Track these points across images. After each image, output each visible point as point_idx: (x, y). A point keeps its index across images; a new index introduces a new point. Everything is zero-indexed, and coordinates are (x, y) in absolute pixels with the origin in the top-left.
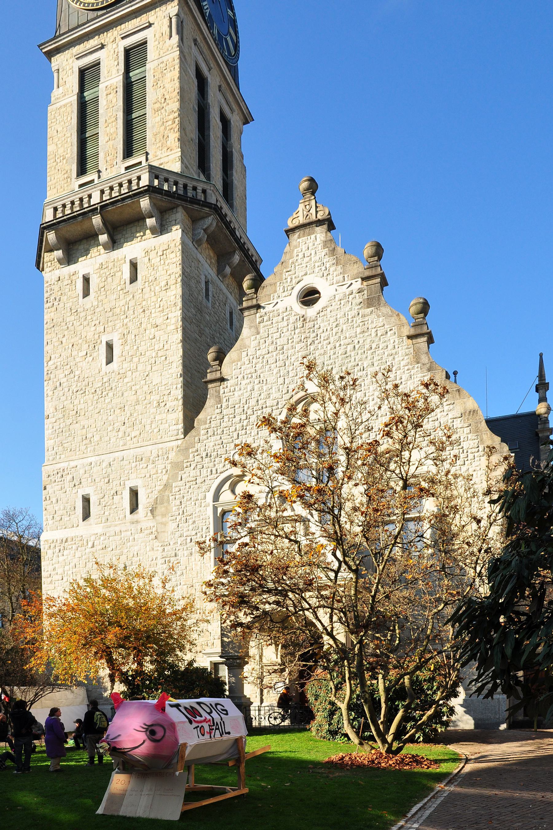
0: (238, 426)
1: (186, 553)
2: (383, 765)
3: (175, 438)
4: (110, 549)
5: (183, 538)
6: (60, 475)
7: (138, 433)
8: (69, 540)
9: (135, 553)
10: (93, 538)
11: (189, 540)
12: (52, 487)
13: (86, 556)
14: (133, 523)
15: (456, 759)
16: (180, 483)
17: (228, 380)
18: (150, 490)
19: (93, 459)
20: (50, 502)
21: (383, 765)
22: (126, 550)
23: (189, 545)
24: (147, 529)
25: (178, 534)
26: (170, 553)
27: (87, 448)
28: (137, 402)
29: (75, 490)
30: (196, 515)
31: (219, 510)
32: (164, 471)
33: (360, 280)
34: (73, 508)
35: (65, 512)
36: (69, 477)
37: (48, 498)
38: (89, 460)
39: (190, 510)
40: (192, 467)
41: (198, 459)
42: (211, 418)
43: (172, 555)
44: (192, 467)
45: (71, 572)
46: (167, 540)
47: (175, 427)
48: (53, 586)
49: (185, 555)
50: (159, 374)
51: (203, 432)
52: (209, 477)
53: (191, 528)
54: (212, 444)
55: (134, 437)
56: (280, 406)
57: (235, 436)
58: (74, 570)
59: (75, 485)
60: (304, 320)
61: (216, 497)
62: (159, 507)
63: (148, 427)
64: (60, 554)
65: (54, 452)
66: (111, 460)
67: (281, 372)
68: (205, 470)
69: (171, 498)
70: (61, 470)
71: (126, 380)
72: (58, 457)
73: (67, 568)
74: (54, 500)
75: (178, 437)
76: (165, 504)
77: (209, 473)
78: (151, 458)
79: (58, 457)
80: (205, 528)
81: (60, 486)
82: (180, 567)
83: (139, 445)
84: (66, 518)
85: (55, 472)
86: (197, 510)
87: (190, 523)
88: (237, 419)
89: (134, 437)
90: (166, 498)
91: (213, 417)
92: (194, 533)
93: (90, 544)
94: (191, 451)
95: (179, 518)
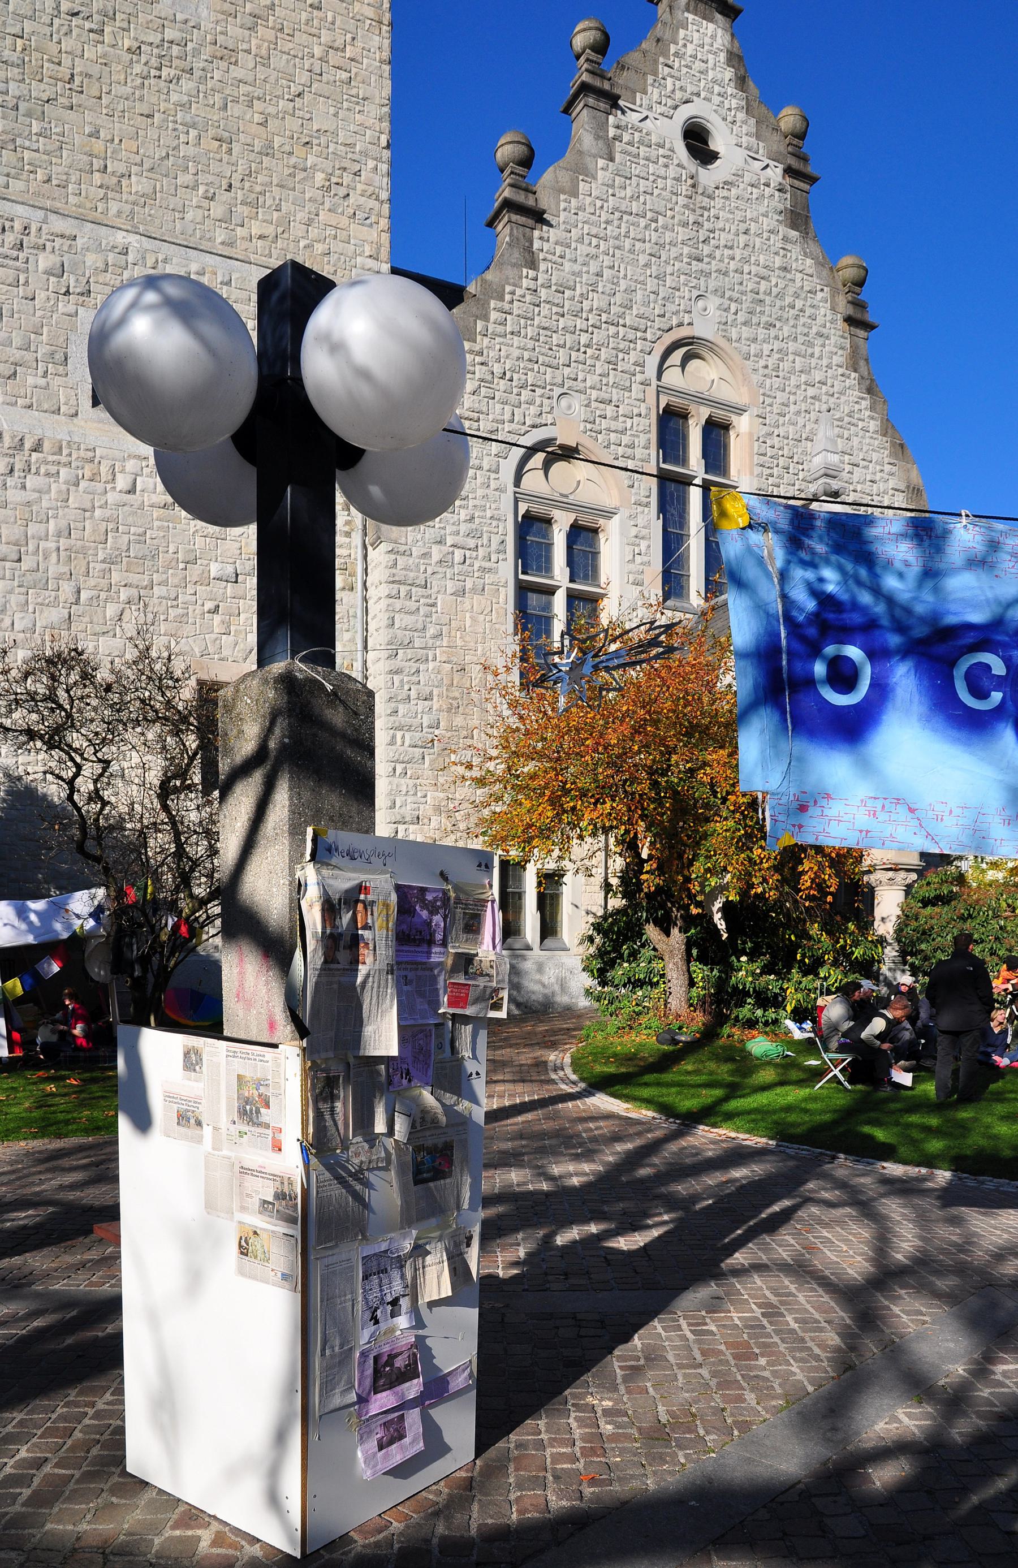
1: (451, 586)
8: (47, 446)
13: (108, 513)
15: (601, 1128)
17: (551, 226)
26: (412, 575)
27: (105, 198)
28: (268, 151)
29: (64, 306)
30: (477, 502)
31: (523, 508)
33: (781, 166)
34: (59, 356)
36: (44, 261)
38: (120, 238)
42: (513, 293)
43: (418, 582)
45: (52, 545)
46: (403, 540)
47: (371, 263)
49: (449, 591)
50: (332, 110)
51: (494, 315)
53: (464, 528)
54: (516, 353)
55: (260, 237)
57: (562, 355)
58: (63, 543)
59: (67, 293)
60: (694, 186)
63: (297, 229)
67: (654, 267)
70: (18, 226)
71: (236, 72)
73: (33, 529)
77: (507, 416)
80: (495, 540)
82: (434, 616)
87: (462, 517)
89: (260, 237)
93: (122, 482)
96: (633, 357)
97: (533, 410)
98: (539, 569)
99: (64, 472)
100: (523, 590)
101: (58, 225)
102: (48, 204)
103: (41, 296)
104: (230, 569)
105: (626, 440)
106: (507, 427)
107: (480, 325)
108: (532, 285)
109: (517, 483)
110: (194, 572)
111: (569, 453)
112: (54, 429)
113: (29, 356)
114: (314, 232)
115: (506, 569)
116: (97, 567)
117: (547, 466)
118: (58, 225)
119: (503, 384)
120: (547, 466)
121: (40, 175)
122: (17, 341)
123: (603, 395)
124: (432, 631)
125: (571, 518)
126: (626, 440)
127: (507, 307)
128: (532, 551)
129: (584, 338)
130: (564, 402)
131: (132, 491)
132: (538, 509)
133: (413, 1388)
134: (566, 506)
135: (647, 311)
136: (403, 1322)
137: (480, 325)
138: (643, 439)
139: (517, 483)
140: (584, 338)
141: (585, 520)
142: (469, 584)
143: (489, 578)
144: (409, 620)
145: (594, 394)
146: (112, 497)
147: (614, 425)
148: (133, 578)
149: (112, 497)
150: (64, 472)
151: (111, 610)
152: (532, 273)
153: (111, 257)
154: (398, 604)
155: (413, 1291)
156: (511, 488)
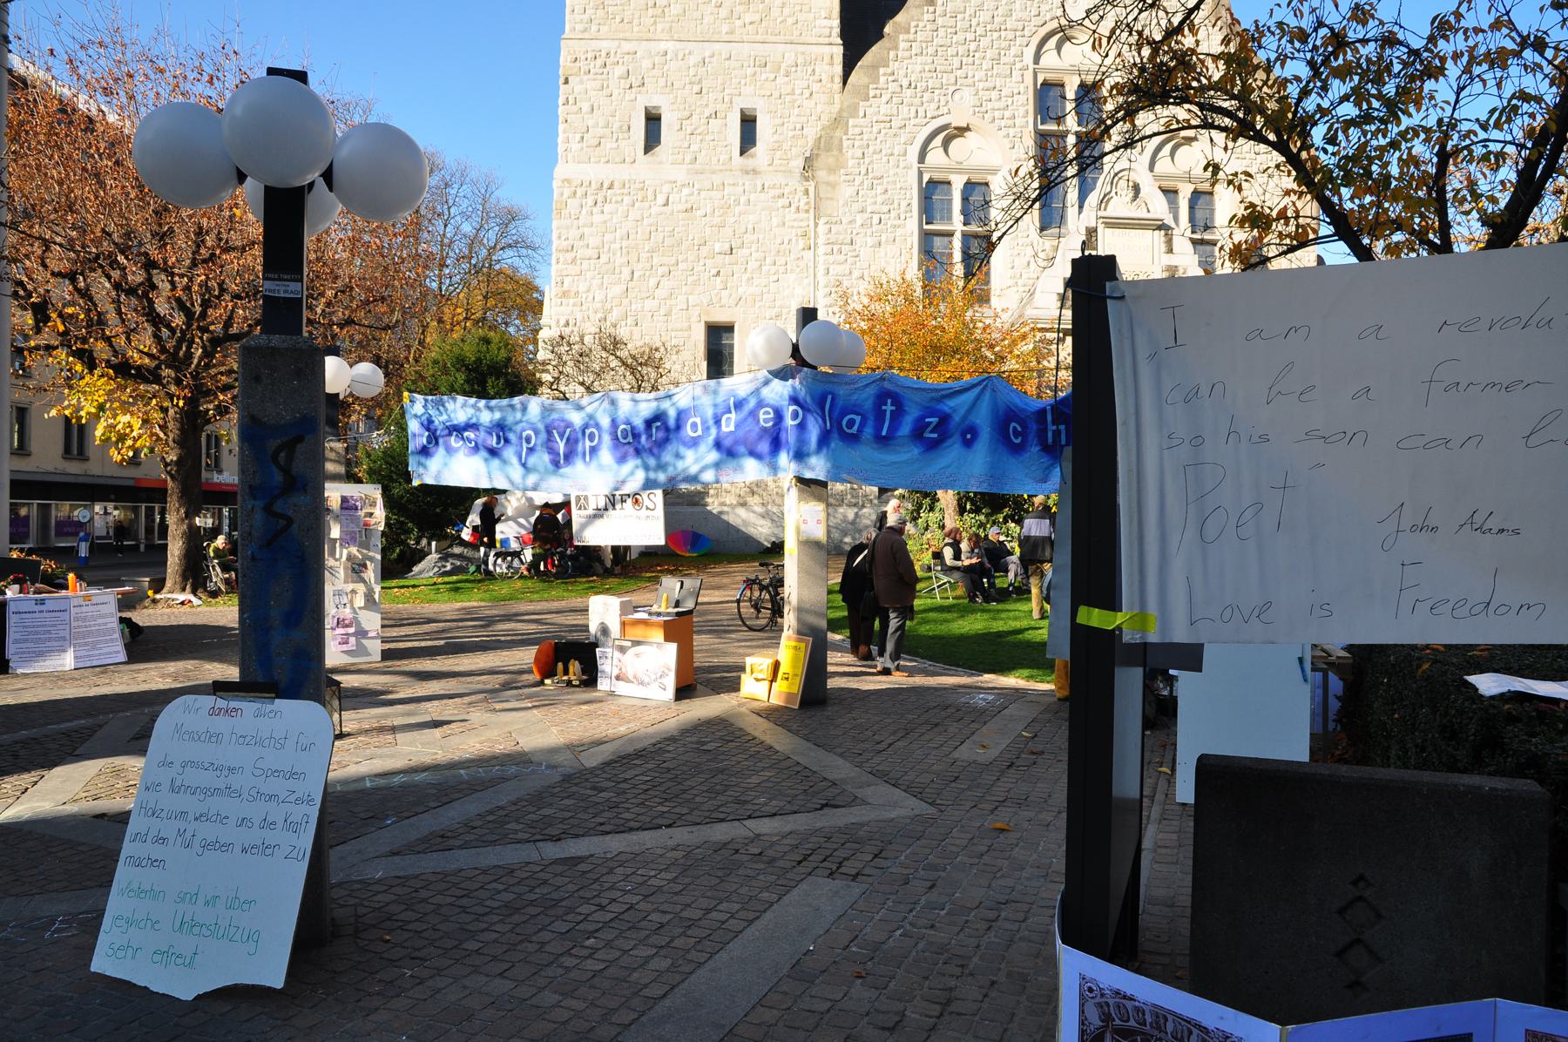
0: (961, 50)
1: (870, 242)
2: (511, 330)
3: (827, 40)
4: (699, 213)
5: (866, 216)
6: (599, 62)
7: (757, 17)
8: (616, 184)
9: (750, 227)
10: (666, 188)
11: (875, 220)
12: (581, 82)
13: (651, 220)
14: (747, 172)
16: (861, 121)
18: (779, 121)
19: (670, 46)
20: (576, 108)
21: (511, 330)
22: (732, 220)
23: (875, 228)
24: (774, 187)
25: (856, 207)
29: (630, 95)
31: (926, 178)
32: (807, 93)
35: (608, 131)
36: (619, 71)
37: (571, 101)
38: (663, 46)
39: (878, 168)
40: (885, 98)
41: (893, 87)
44: (885, 98)
47: (826, 23)
48: (577, 268)
51: (902, 45)
52: (913, 122)
53: (880, 199)
54: (919, 68)
56: (1026, 33)
57: (956, 64)
58: (625, 243)
61: (922, 157)
62: (823, 155)
63: (775, 12)
64: (595, 210)
65: (586, 17)
66: (707, 54)
68: (906, 109)
69: (845, 143)
70: (603, 54)
72: (594, 28)
73: (608, 237)
74: (586, 107)
75: (831, 40)
76: (835, 152)
77: (913, 114)
78: (783, 66)
79: (594, 28)
80: (904, 204)
81: (599, 83)
83: (759, 38)
84: (609, 145)
85: (590, 55)
86: (891, 172)
88: (960, 37)
90: (836, 142)
91: (921, 24)
92: (885, 209)
93: (661, 199)
94: (882, 71)
95: (858, 180)
96: (1013, 51)
97: (933, 106)
98: (942, 218)
99: (626, 199)
100: (926, 237)
101: (627, 46)
102: (621, 35)
103: (615, 93)
104: (727, 246)
105: (1007, 114)
106: (913, 122)
107: (892, 54)
108: (931, 17)
109: (1037, 60)
110: (704, 251)
111: (962, 131)
112: (619, 173)
113: (608, 131)
114: (786, 11)
115: (911, 226)
116: (644, 256)
117: (1059, 48)
118: (627, 46)
119: (909, 92)
120: (1059, 48)
121: (618, 19)
122: (602, 123)
123: (988, 85)
124: (856, 274)
125: (964, 179)
126: (1007, 114)
127: (911, 37)
128: (937, 206)
129: (973, 46)
130: (957, 96)
131: (666, 204)
132: (937, 176)
133: (351, 630)
134: (959, 171)
135: (1024, 15)
136: (348, 610)
137: (892, 54)
138: (1022, 111)
139: (1037, 60)
140: (973, 46)
141: (976, 178)
142: (883, 239)
143: (899, 232)
144: (840, 269)
145: (981, 85)
146: (654, 210)
147: (997, 105)
148: (666, 260)
149: (654, 210)
150: (626, 199)
151: (653, 282)
152: (931, 9)
153: (657, 60)
154: (831, 258)
155: (351, 602)
156: (916, 165)
